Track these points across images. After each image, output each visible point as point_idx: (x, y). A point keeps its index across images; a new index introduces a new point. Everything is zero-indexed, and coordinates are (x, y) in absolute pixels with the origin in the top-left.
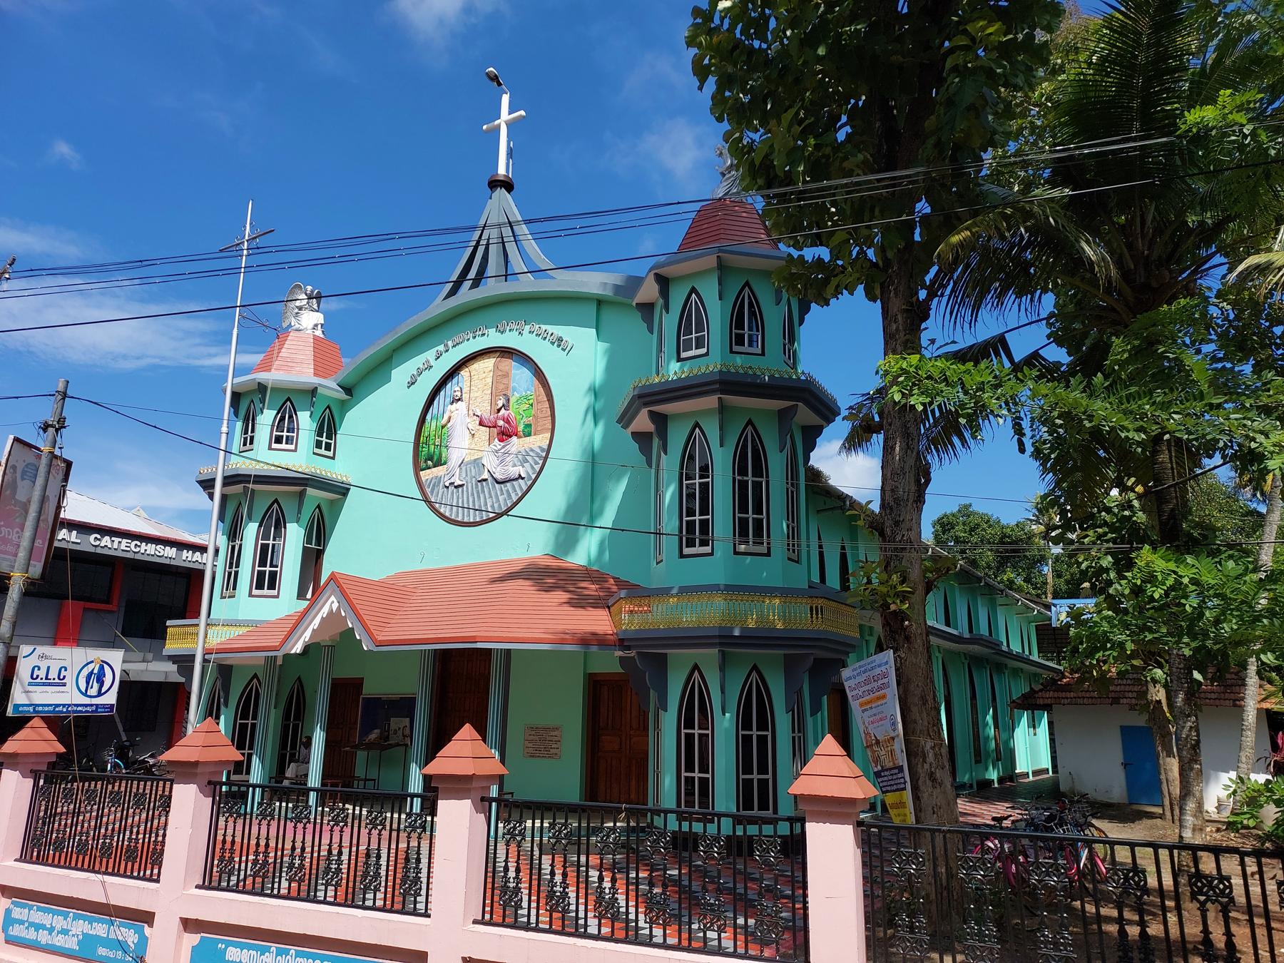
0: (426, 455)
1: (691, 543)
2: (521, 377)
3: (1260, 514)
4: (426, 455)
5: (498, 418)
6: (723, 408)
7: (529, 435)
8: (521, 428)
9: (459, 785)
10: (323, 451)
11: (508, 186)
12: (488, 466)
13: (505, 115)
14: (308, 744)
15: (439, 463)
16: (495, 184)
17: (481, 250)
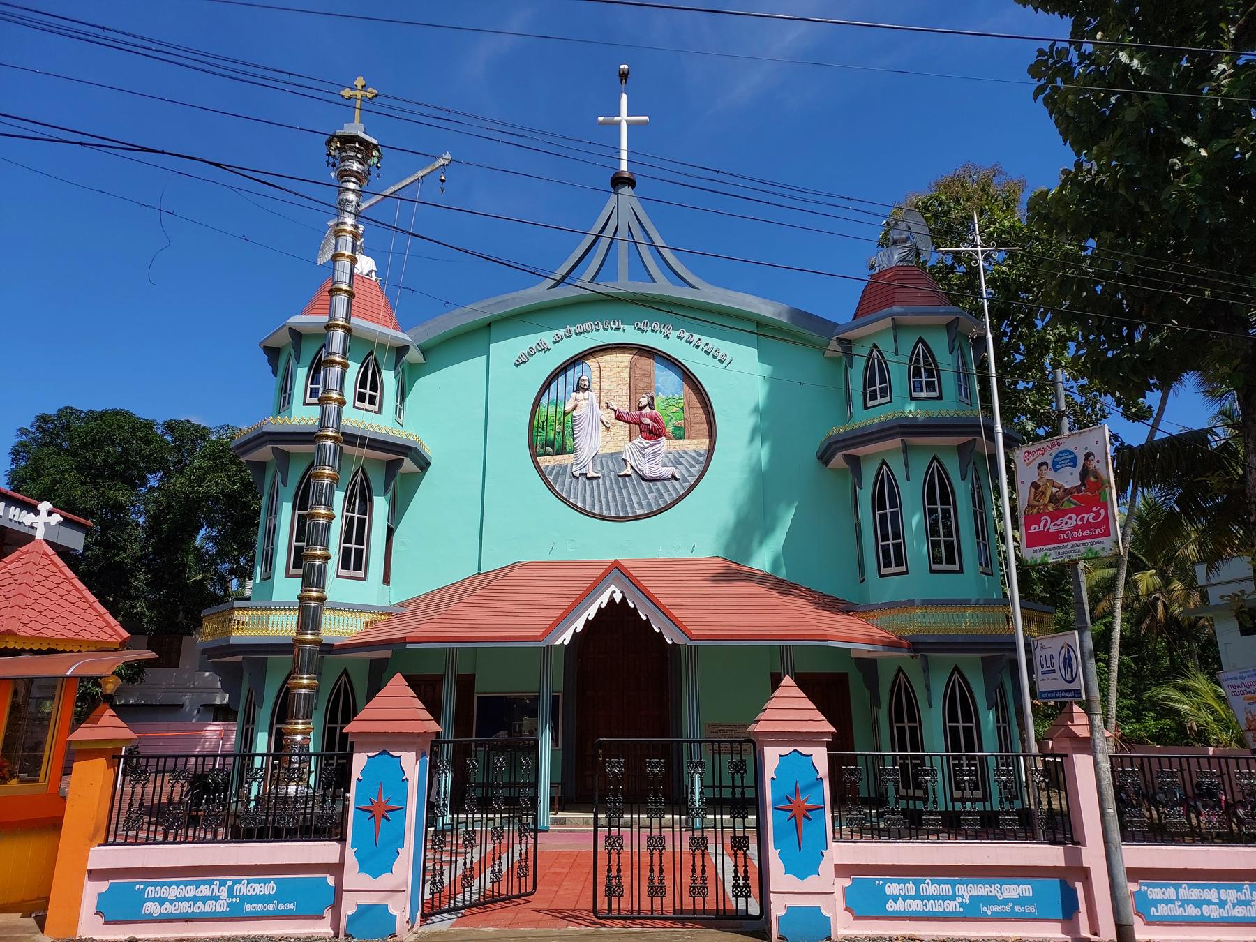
0: (547, 440)
1: (888, 565)
2: (666, 381)
3: (1129, 836)
4: (547, 440)
5: (641, 415)
6: (906, 448)
7: (681, 438)
8: (669, 429)
9: (89, 751)
10: (366, 405)
11: (631, 183)
12: (630, 461)
13: (624, 117)
14: (534, 749)
15: (562, 451)
16: (618, 181)
17: (603, 244)
